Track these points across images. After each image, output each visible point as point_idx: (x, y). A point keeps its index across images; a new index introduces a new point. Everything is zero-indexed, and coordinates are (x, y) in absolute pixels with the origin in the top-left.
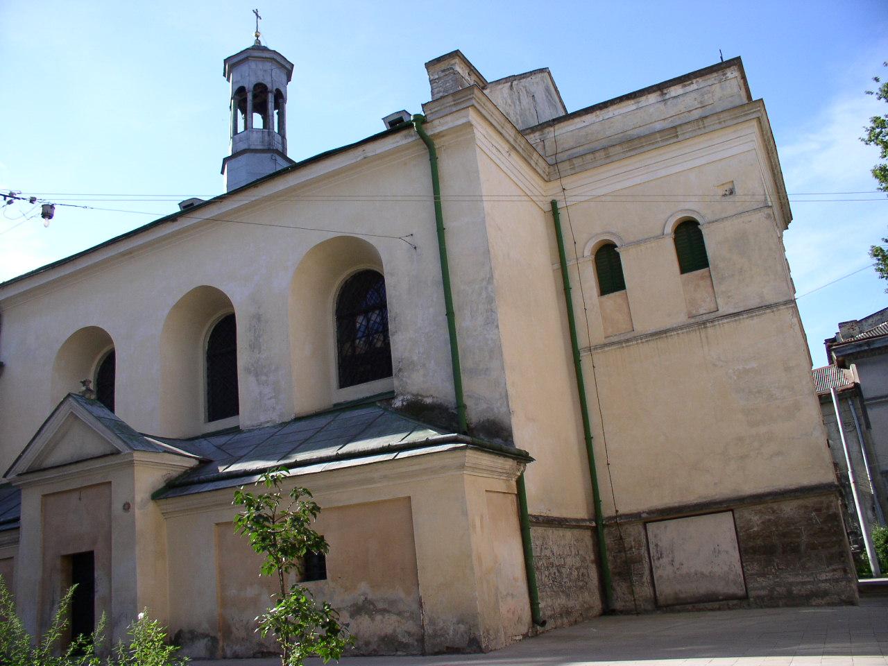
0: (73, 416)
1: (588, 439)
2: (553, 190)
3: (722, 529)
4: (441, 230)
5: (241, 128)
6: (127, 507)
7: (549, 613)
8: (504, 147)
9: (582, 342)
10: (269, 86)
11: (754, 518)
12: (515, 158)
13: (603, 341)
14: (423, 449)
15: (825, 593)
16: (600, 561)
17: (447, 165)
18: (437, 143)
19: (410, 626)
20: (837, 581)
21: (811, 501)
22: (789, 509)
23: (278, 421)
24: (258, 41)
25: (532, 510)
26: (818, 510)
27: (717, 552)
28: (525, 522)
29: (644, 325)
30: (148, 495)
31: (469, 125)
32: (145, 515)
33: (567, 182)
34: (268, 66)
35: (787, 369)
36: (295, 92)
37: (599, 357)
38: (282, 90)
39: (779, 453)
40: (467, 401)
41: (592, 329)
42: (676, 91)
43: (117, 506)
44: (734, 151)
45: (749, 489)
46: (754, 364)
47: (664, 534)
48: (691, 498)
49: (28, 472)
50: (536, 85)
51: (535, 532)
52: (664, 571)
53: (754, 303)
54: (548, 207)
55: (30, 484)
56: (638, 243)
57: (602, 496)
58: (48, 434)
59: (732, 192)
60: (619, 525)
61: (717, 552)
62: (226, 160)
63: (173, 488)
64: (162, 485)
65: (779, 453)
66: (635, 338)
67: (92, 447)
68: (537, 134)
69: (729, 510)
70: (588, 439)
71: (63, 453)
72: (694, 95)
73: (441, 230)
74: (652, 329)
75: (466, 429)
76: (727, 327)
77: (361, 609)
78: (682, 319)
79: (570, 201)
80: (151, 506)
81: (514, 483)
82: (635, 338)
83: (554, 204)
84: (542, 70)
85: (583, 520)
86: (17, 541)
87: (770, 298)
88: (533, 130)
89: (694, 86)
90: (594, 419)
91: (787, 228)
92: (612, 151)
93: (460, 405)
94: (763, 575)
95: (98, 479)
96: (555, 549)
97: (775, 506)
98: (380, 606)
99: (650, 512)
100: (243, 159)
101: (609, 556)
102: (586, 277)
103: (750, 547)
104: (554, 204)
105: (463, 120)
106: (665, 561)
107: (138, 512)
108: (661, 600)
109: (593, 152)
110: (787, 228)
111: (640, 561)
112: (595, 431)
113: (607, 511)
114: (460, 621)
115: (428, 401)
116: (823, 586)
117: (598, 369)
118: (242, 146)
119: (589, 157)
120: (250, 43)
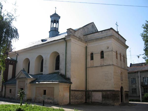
0: (22, 72)
1: (86, 79)
2: (86, 45)
3: (100, 94)
4: (66, 53)
5: (52, 27)
6: (27, 84)
7: (71, 102)
8: (77, 41)
9: (87, 67)
10: (56, 20)
11: (104, 93)
12: (79, 42)
13: (90, 67)
14: (7, 103)
15: (111, 104)
16: (86, 96)
17: (68, 44)
18: (67, 41)
19: (53, 101)
20: (112, 103)
21: (111, 92)
22: (108, 93)
23: (47, 74)
24: (55, 12)
25: (71, 89)
26: (112, 93)
27: (99, 97)
28: (70, 90)
29: (95, 65)
30: (29, 83)
31: (70, 39)
32: (28, 85)
33: (88, 44)
34: (56, 17)
35: (111, 74)
36: (60, 20)
37: (89, 69)
38: (58, 20)
39: (108, 85)
40: (66, 75)
41: (89, 65)
42: (103, 32)
43: (26, 84)
44: (109, 42)
45: (104, 89)
46: (107, 73)
47: (94, 93)
48: (97, 89)
49: (17, 78)
50: (92, 24)
51: (71, 92)
52: (93, 98)
53: (108, 64)
54: (85, 47)
55: (17, 80)
56: (96, 54)
57: (87, 87)
58: (20, 74)
59: (108, 48)
60: (88, 91)
61: (99, 97)
62: (49, 32)
63: (32, 82)
64: (31, 81)
65: (108, 85)
66: (94, 67)
67: (24, 77)
68: (86, 36)
69: (101, 92)
70: (86, 79)
71: (20, 77)
72: (106, 33)
73: (66, 53)
74: (96, 66)
75: (65, 78)
76: (105, 67)
77: (49, 99)
78: (99, 65)
79: (88, 46)
80: (29, 84)
81: (69, 86)
82: (94, 67)
83: (86, 46)
84: (92, 23)
85: (84, 90)
86: (16, 85)
87: (111, 64)
88: (85, 35)
89: (106, 32)
90: (87, 77)
91: (127, 47)
92: (94, 40)
93: (66, 75)
94: (104, 101)
95: (24, 80)
96: (76, 94)
97: (107, 92)
98: (50, 99)
99: (92, 90)
100: (51, 32)
101: (87, 95)
102: (89, 58)
103: (103, 97)
104: (86, 46)
105: (69, 39)
106: (93, 97)
107: (28, 84)
108: (92, 102)
109: (91, 40)
110: (127, 47)
111: (90, 96)
112: (87, 79)
113: (87, 89)
114: (57, 102)
115: (63, 74)
116: (111, 103)
117: (89, 70)
118: (52, 30)
119: (91, 41)
120: (54, 13)
